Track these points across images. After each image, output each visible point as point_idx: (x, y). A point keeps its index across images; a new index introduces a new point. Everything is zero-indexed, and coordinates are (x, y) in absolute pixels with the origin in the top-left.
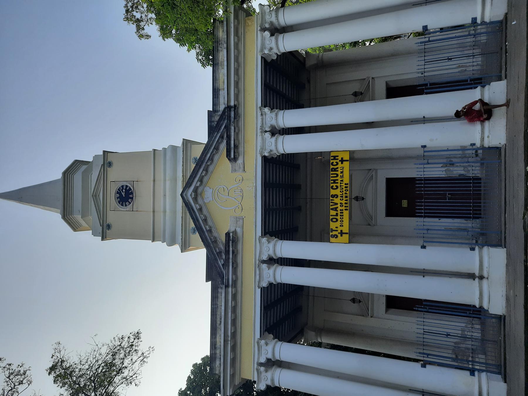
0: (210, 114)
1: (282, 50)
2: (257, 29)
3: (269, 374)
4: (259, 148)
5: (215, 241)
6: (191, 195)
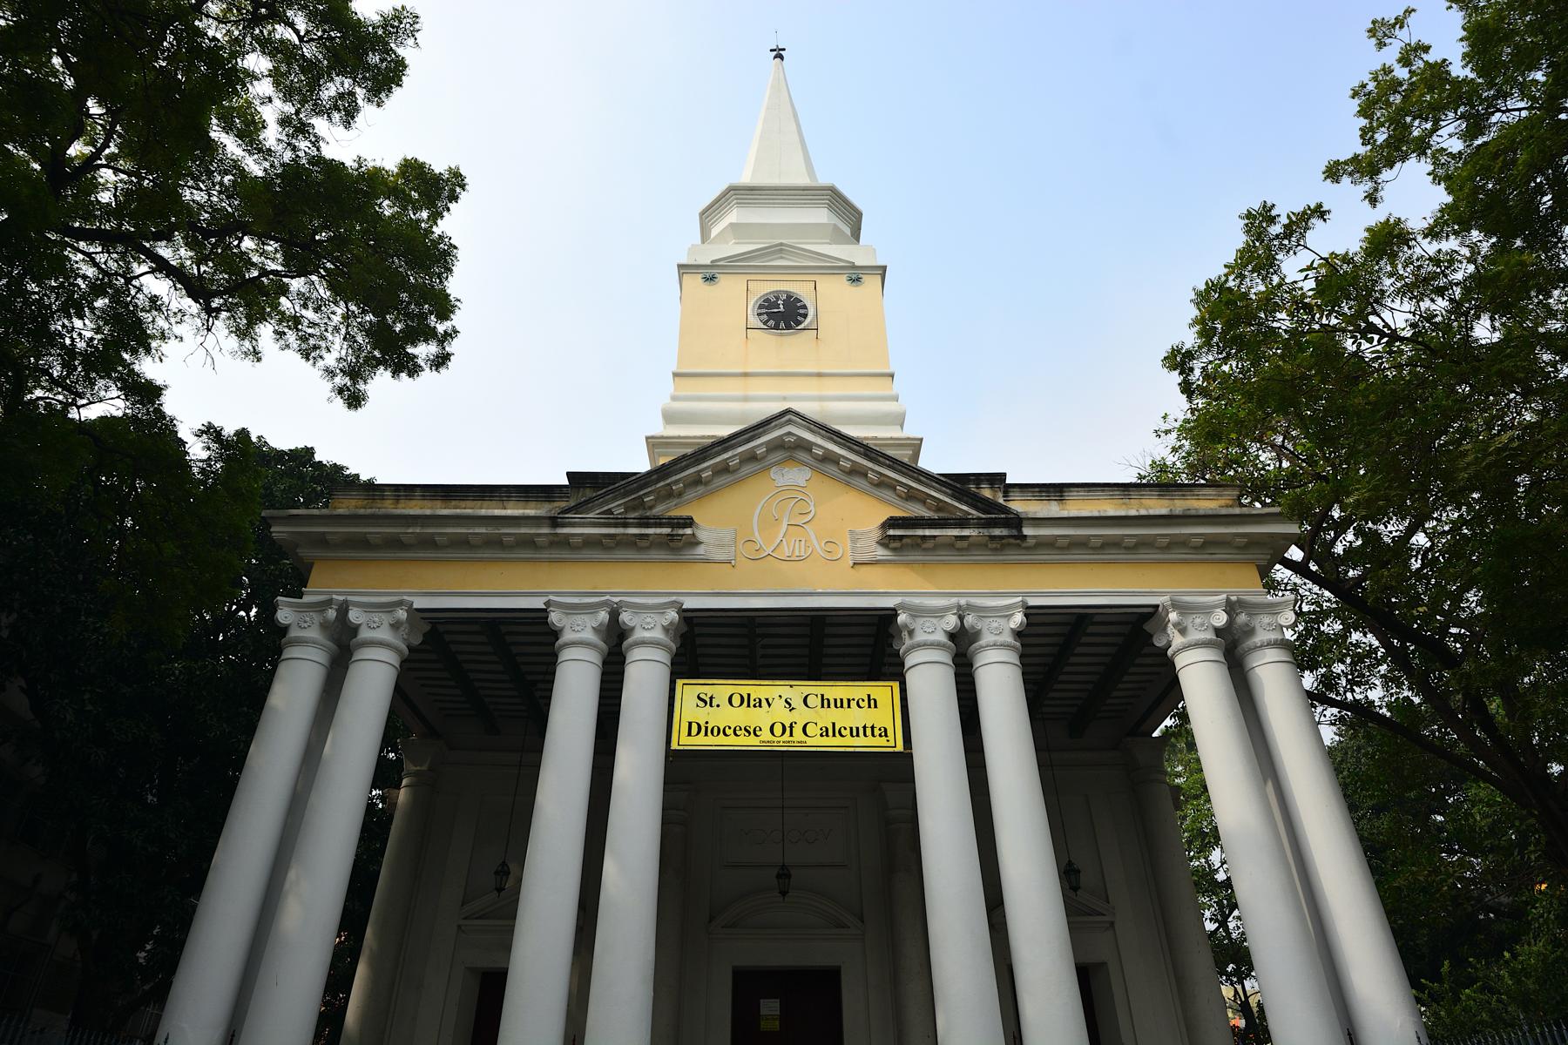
0: (997, 479)
1: (1180, 661)
2: (1233, 593)
3: (313, 633)
4: (917, 601)
5: (670, 495)
6: (789, 433)
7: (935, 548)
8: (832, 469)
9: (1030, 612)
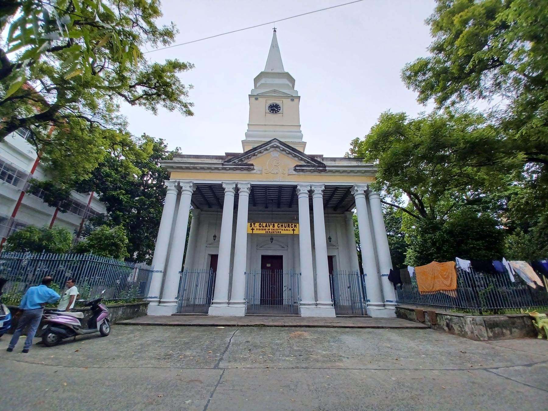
0: (321, 156)
3: (173, 188)
8: (284, 152)
9: (326, 186)
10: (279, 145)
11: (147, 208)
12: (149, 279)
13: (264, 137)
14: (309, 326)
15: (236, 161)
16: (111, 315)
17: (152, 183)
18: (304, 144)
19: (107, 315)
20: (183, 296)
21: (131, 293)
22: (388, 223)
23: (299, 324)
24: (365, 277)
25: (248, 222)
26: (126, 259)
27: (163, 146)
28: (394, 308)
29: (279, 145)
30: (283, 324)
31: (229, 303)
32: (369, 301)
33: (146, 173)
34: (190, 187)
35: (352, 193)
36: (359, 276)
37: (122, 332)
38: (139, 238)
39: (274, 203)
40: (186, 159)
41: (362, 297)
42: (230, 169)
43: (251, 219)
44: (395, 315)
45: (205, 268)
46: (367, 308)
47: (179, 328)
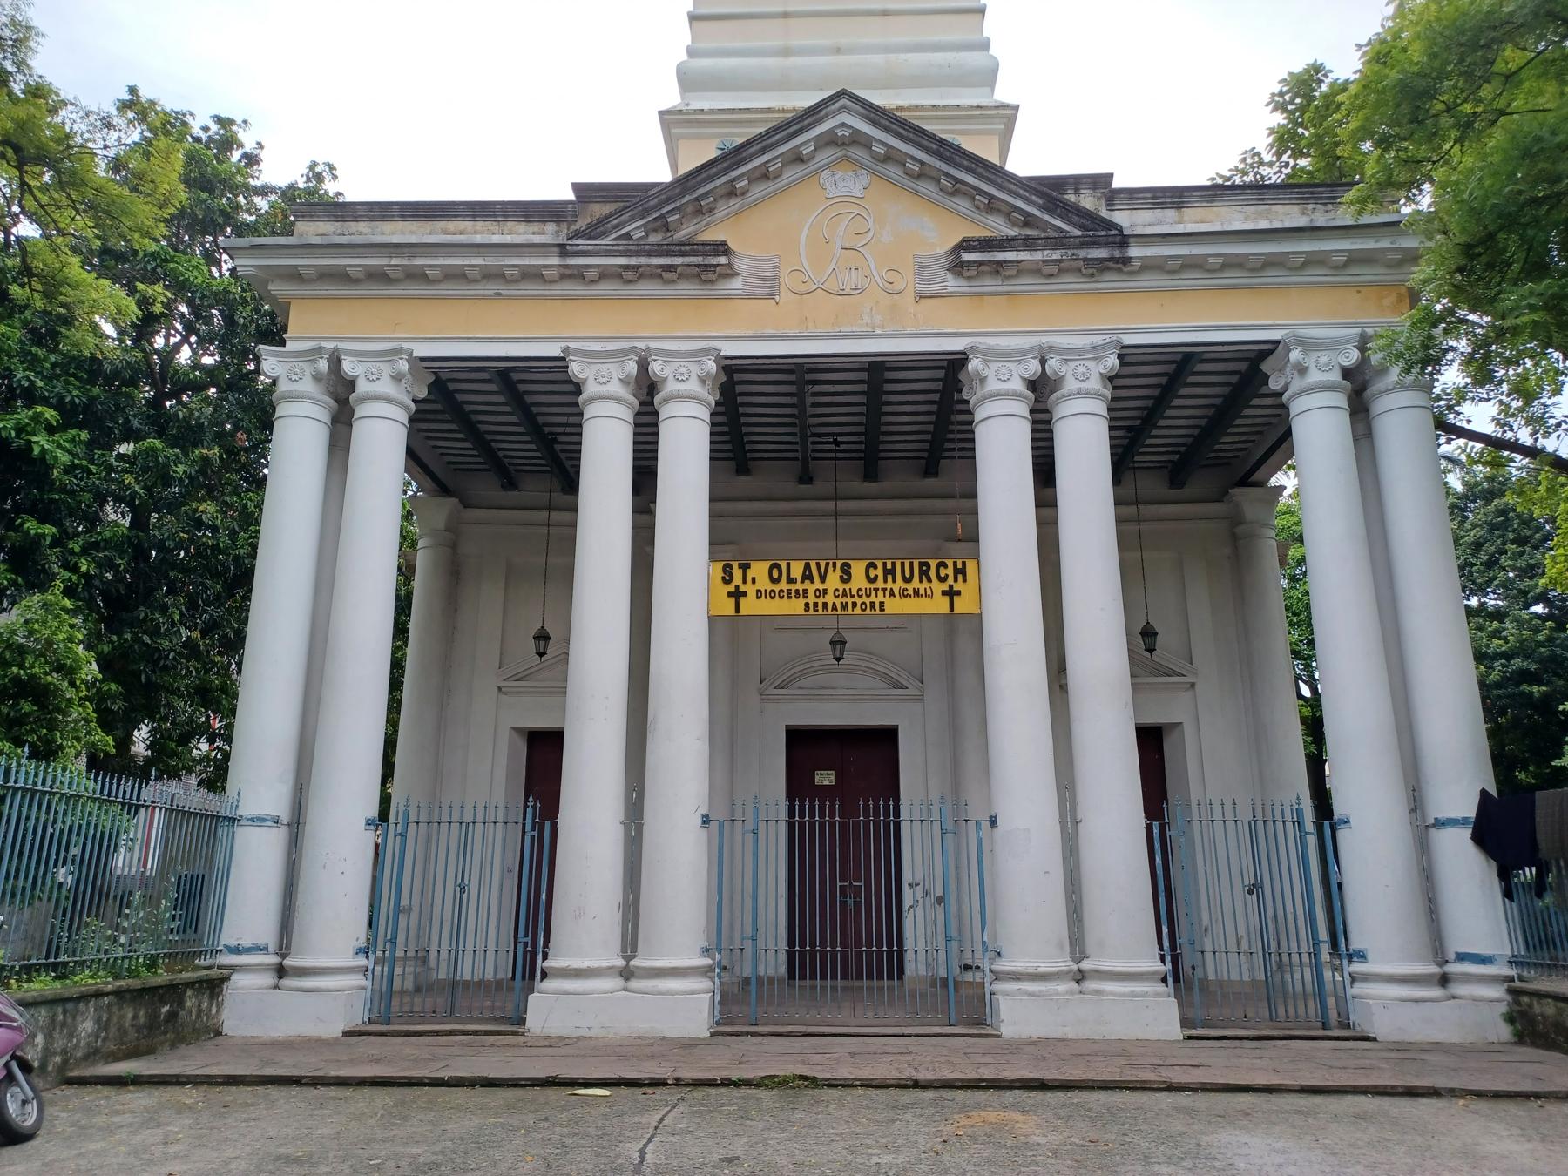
0: (1100, 183)
3: (307, 386)
4: (991, 342)
6: (843, 125)
7: (1019, 273)
8: (894, 171)
10: (866, 128)
11: (186, 496)
12: (219, 858)
13: (783, 84)
14: (1043, 1086)
15: (635, 228)
16: (40, 1039)
17: (196, 365)
18: (1006, 116)
19: (18, 1038)
20: (393, 941)
21: (134, 928)
22: (1478, 546)
23: (987, 1073)
24: (1342, 835)
25: (713, 558)
26: (96, 763)
27: (236, 155)
28: (1497, 992)
29: (866, 128)
30: (909, 1074)
31: (627, 974)
32: (1362, 956)
33: (158, 309)
34: (397, 378)
35: (1274, 384)
36: (1309, 826)
37: (101, 1120)
38: (153, 656)
39: (847, 450)
40: (362, 226)
41: (1323, 934)
42: (605, 275)
43: (728, 546)
44: (1504, 1032)
45: (499, 796)
46: (1351, 991)
47: (385, 1097)
